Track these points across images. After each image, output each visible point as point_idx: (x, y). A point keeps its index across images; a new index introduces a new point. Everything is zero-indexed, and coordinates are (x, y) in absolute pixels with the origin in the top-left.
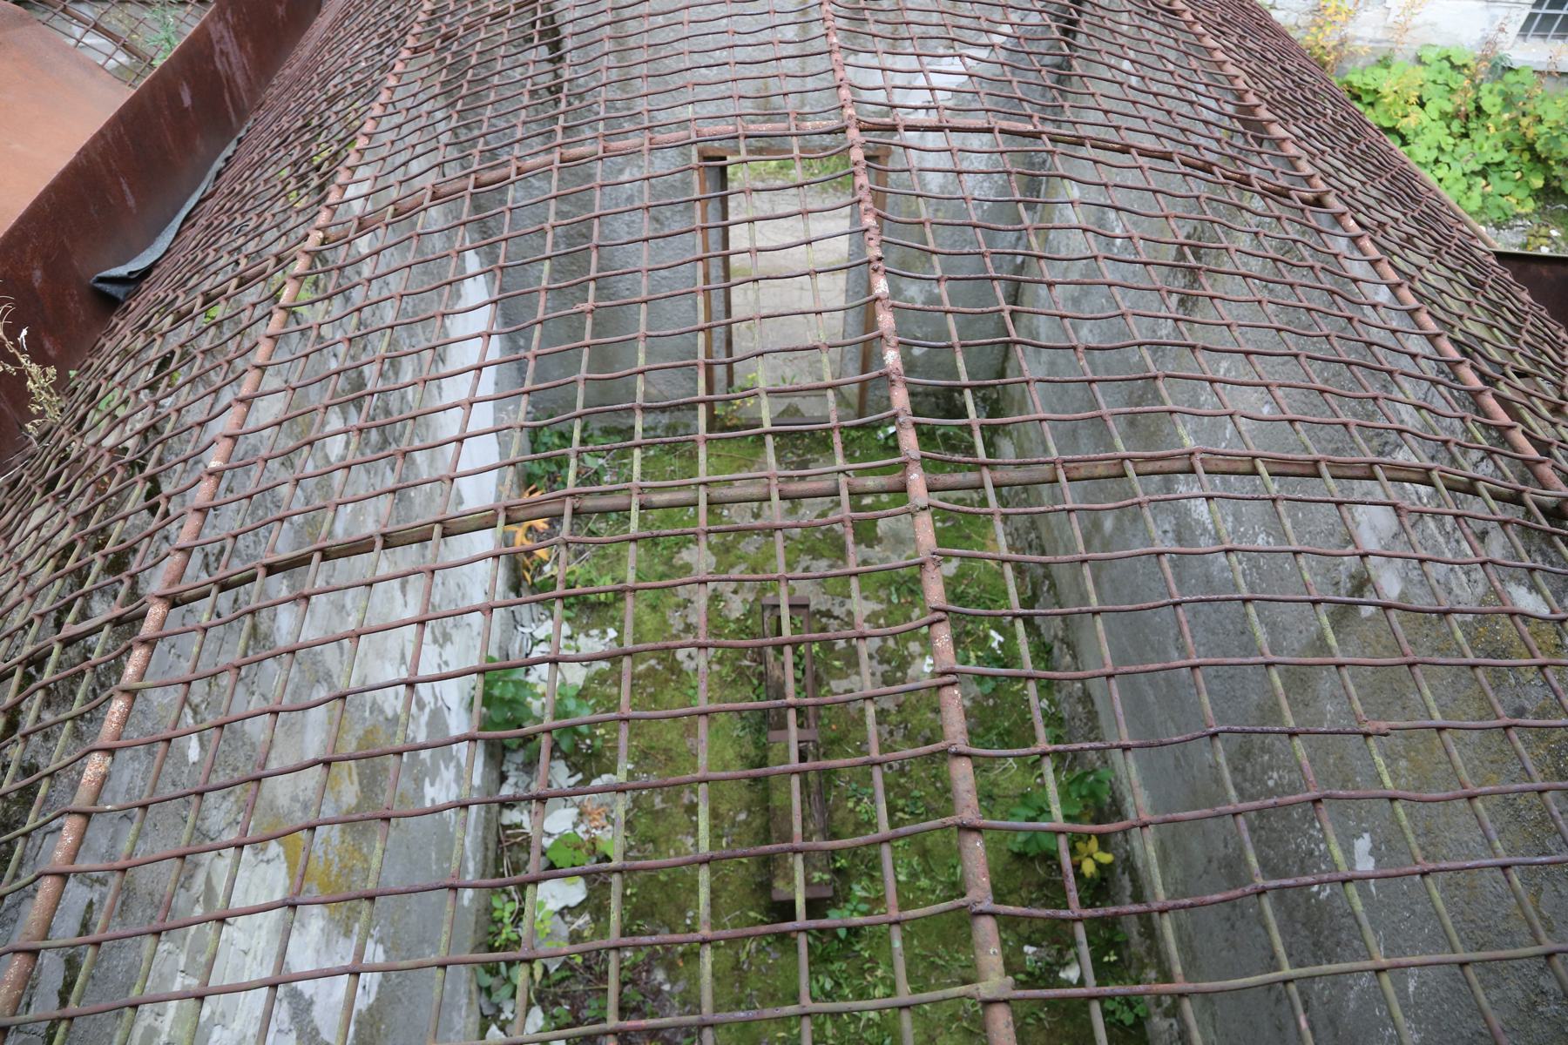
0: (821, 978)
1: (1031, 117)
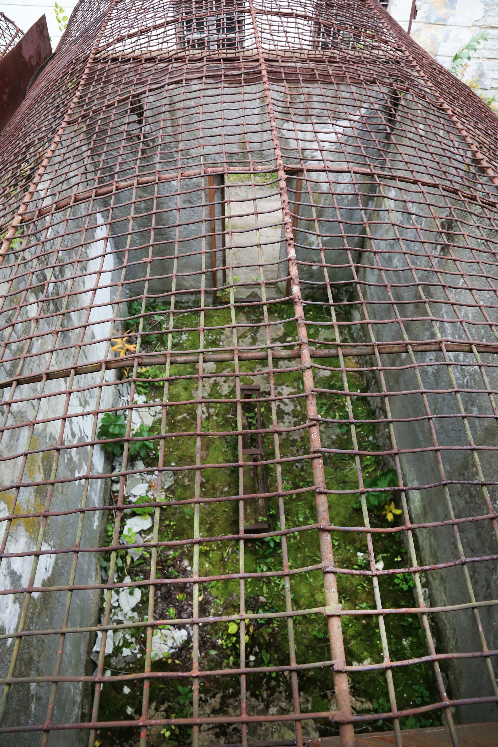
0: (262, 566)
1: (369, 165)
